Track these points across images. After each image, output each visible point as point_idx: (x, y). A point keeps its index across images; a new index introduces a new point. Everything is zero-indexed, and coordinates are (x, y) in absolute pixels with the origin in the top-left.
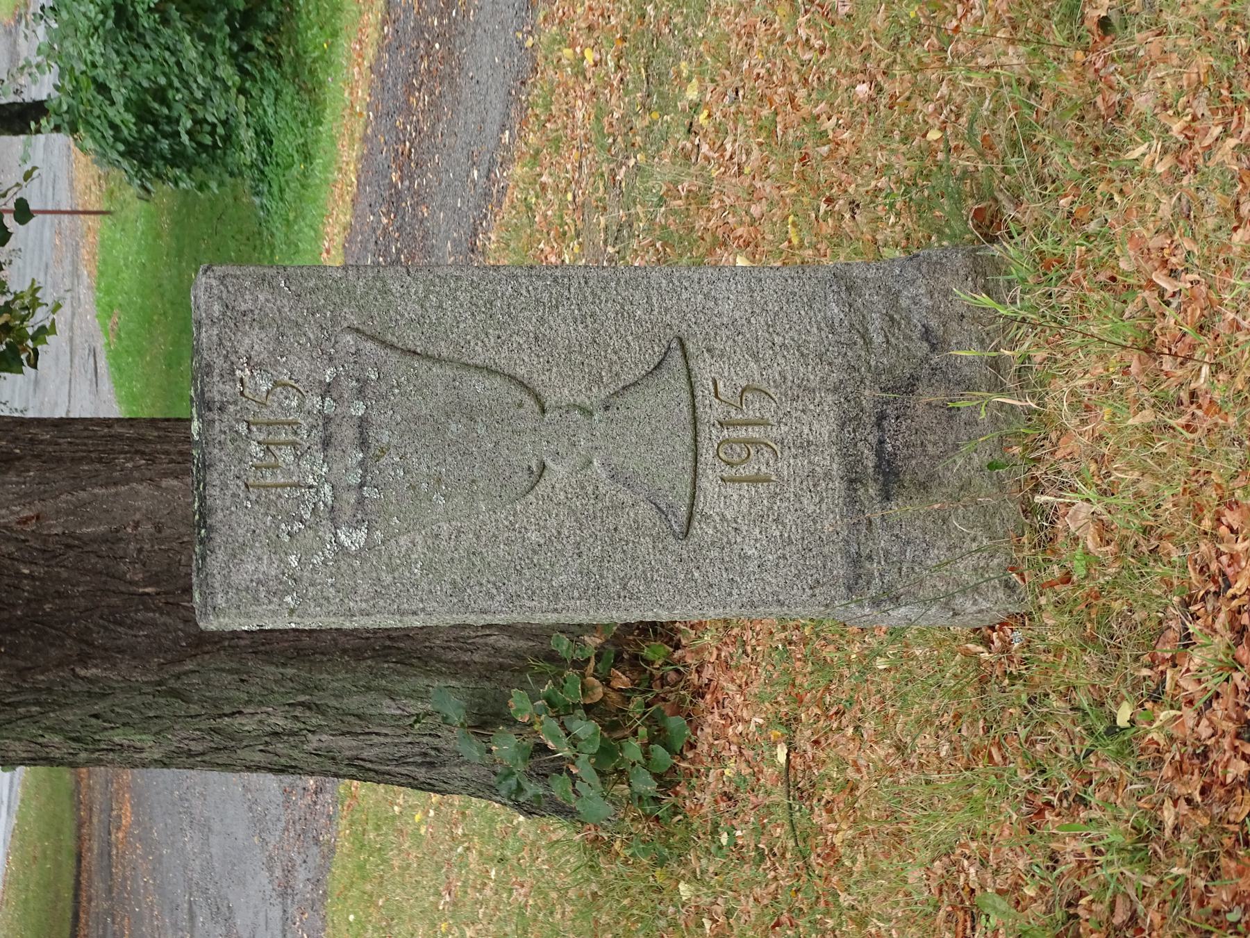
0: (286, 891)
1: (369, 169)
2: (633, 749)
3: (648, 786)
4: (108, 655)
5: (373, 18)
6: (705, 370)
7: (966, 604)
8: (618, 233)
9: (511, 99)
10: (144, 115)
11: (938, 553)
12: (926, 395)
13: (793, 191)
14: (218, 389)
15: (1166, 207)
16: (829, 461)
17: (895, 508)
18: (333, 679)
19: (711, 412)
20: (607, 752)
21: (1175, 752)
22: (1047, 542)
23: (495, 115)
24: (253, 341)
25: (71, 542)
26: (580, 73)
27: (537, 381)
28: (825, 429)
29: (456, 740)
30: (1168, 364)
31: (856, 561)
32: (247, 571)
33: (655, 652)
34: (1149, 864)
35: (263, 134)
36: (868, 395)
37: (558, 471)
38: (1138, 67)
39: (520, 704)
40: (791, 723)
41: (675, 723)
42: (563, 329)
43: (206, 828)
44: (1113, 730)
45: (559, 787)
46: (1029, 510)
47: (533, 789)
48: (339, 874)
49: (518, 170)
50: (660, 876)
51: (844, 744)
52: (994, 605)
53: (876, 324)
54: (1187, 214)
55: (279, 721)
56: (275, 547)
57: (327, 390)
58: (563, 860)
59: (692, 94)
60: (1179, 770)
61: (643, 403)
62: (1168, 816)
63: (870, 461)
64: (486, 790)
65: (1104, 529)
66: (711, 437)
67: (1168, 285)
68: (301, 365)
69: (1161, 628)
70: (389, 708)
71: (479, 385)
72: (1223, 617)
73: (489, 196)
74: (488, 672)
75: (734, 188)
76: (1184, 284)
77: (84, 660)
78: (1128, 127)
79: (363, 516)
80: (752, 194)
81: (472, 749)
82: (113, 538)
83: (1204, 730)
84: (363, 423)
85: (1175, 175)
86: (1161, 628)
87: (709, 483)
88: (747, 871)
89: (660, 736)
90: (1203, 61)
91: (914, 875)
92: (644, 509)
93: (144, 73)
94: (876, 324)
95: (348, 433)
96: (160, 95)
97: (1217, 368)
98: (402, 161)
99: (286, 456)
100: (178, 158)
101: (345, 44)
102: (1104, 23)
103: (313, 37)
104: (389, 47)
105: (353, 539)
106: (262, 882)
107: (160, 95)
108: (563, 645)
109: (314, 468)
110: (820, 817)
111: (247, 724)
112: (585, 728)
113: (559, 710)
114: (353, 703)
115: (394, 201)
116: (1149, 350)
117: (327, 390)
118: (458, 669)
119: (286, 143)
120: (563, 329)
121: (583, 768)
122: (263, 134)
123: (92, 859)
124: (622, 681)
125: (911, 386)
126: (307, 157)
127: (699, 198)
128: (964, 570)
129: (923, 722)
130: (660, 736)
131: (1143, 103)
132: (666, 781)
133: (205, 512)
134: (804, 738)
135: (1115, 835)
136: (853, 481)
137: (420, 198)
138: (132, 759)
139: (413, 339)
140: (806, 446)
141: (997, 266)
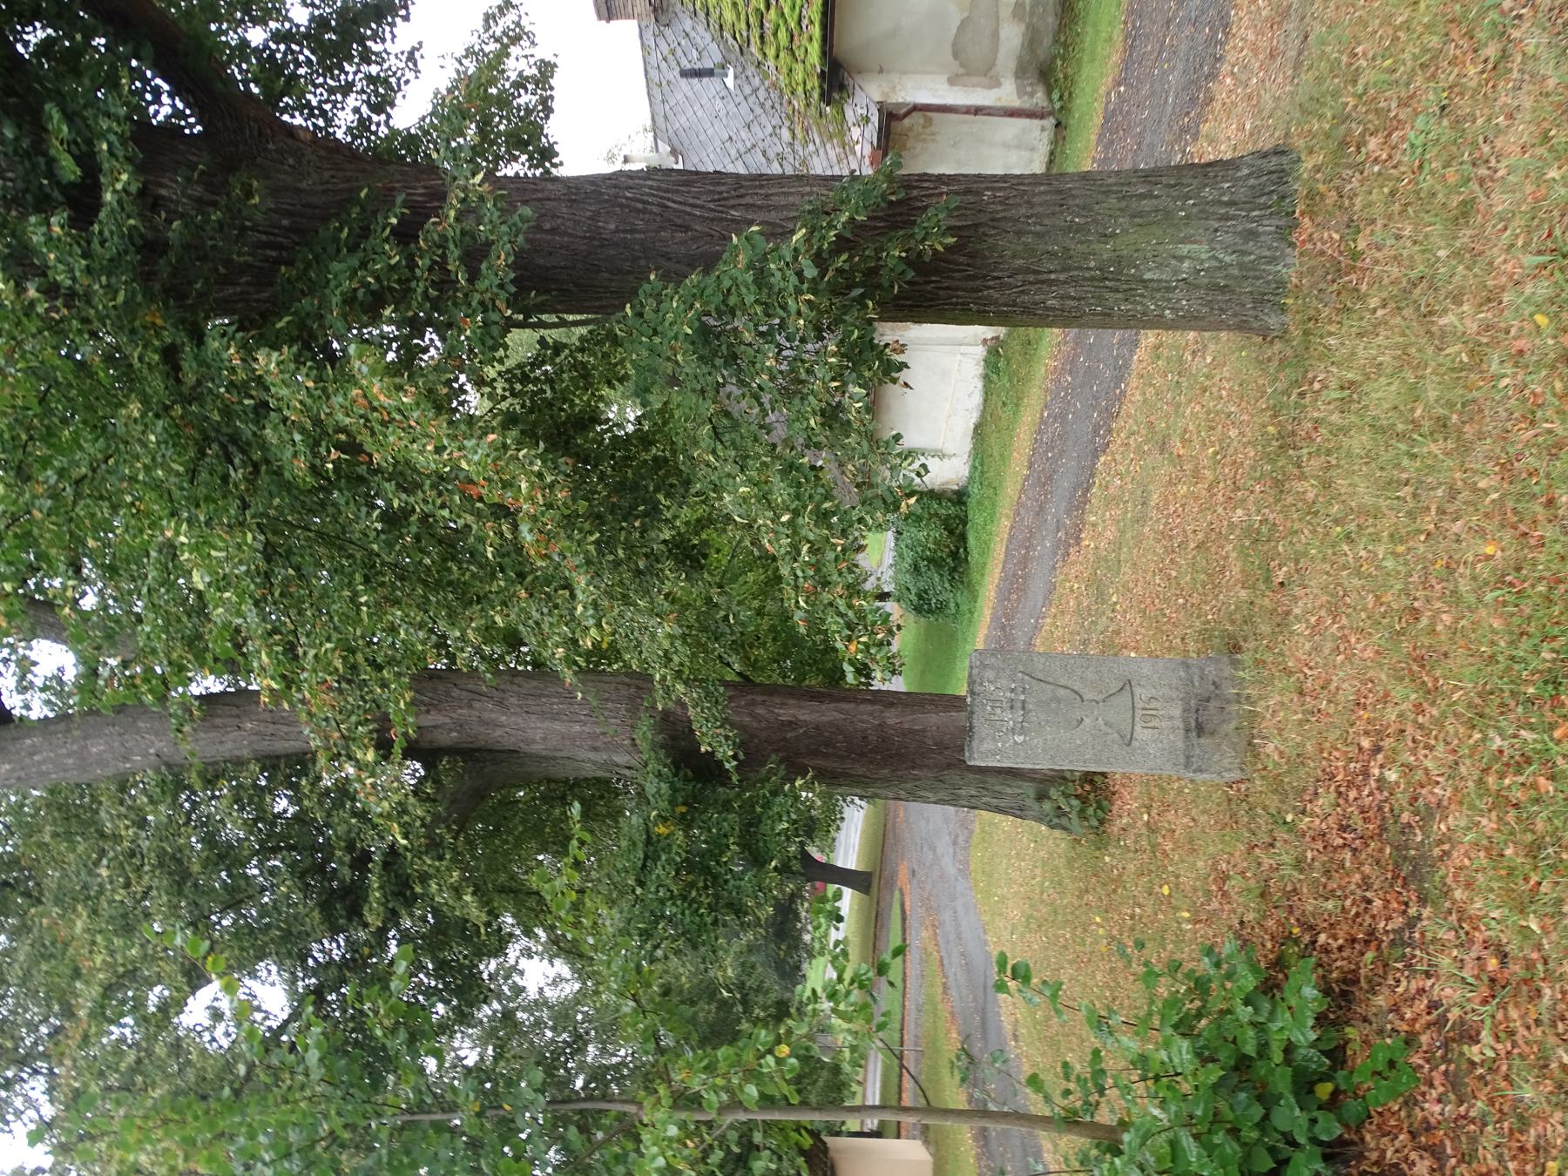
0: (955, 843)
1: (994, 618)
2: (1090, 811)
3: (1095, 823)
4: (921, 767)
5: (998, 570)
6: (1137, 691)
7: (1226, 775)
8: (1085, 642)
9: (1046, 598)
10: (920, 597)
11: (1216, 757)
12: (1213, 704)
13: (222, 554)
14: (977, 689)
15: (1308, 646)
16: (1179, 723)
17: (1202, 741)
18: (991, 780)
19: (1139, 705)
20: (1082, 811)
21: (1311, 833)
22: (1257, 756)
23: (1040, 603)
24: (989, 674)
25: (911, 731)
26: (1072, 590)
27: (1081, 691)
28: (1177, 712)
29: (1030, 802)
30: (1308, 699)
31: (1188, 757)
32: (985, 747)
33: (1098, 779)
34: (1301, 871)
35: (957, 605)
36: (1193, 703)
37: (1087, 721)
38: (1296, 599)
39: (1053, 793)
40: (1149, 808)
41: (1105, 803)
42: (1090, 675)
43: (928, 820)
44: (1285, 823)
45: (1064, 821)
46: (1250, 744)
47: (1056, 821)
48: (975, 839)
49: (1048, 620)
50: (1097, 853)
51: (1170, 816)
52: (1236, 775)
53: (1196, 679)
54: (1316, 649)
55: (973, 792)
56: (994, 739)
57: (1012, 691)
58: (1417, 935)
59: (1114, 599)
60: (1313, 839)
61: (1116, 700)
62: (1309, 855)
63: (1193, 724)
64: (1039, 820)
65: (1281, 754)
66: (1139, 713)
67: (1309, 672)
68: (1004, 682)
69: (1304, 790)
70: (1009, 791)
71: (1062, 692)
72: (1332, 789)
73: (1037, 628)
74: (1042, 781)
75: (1129, 630)
76: (1315, 672)
77: (913, 768)
78: (1291, 618)
79: (1023, 731)
80: (1137, 633)
81: (1036, 806)
82: (924, 730)
83: (1324, 826)
84: (1024, 702)
85: (1312, 636)
86: (1304, 790)
87: (1138, 728)
88: (1131, 855)
89: (1100, 807)
90: (1325, 598)
91: (1200, 864)
92: (1116, 735)
93: (921, 585)
94: (1196, 679)
95: (1019, 705)
96: (926, 592)
97: (1330, 702)
98: (1006, 615)
99: (998, 711)
100: (930, 611)
101: (987, 578)
102: (1282, 584)
103: (975, 576)
104: (1001, 579)
105: (1019, 739)
106: (947, 839)
107: (926, 592)
108: (1068, 775)
109: (1007, 715)
110: (1160, 840)
111: (963, 792)
112: (1075, 802)
113: (1066, 796)
114: (998, 788)
115: (1003, 628)
116: (1301, 693)
117: (1012, 691)
118: (1032, 780)
119: (964, 608)
120: (1090, 675)
121: (1073, 816)
122: (957, 605)
123: (889, 825)
124: (1088, 788)
125: (1208, 700)
126: (971, 613)
127: (1117, 633)
128: (1225, 762)
129: (1204, 812)
130: (1100, 807)
131: (1297, 611)
132: (1102, 822)
133: (971, 728)
134: (1154, 812)
135: (1286, 859)
136: (1187, 731)
137: (1012, 627)
138: (925, 800)
139: (1040, 676)
140: (1171, 718)
141: (1239, 661)
